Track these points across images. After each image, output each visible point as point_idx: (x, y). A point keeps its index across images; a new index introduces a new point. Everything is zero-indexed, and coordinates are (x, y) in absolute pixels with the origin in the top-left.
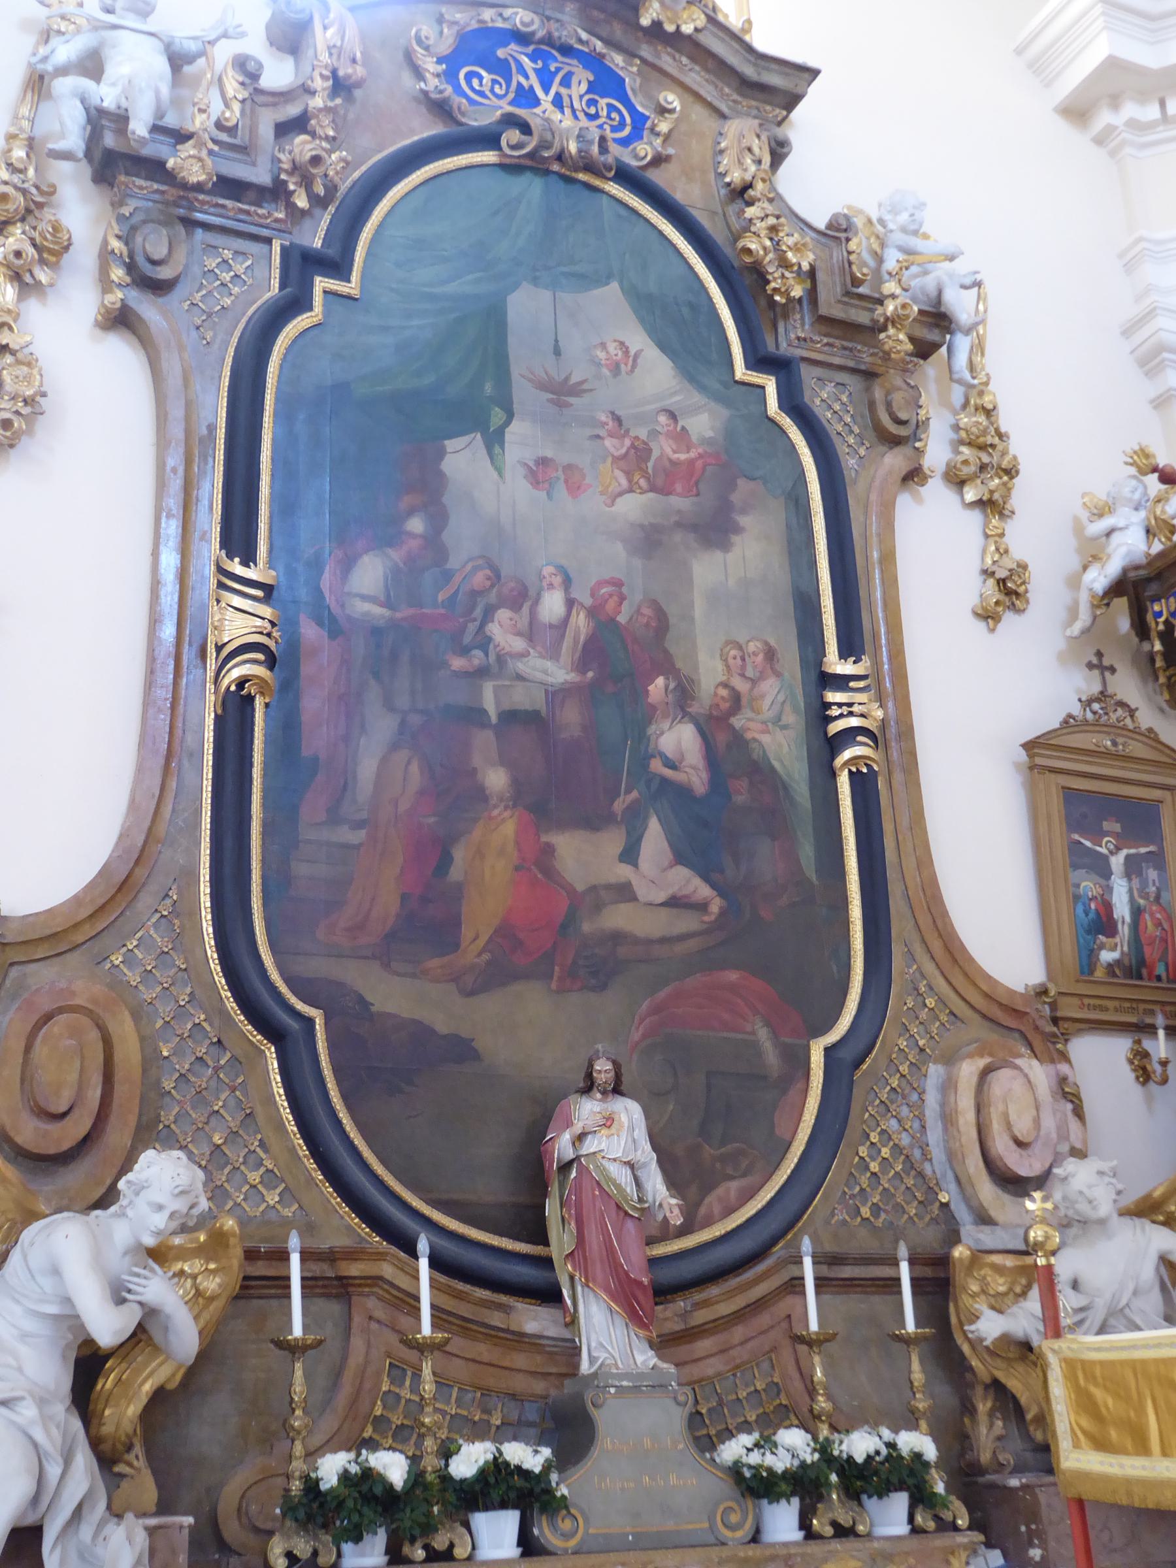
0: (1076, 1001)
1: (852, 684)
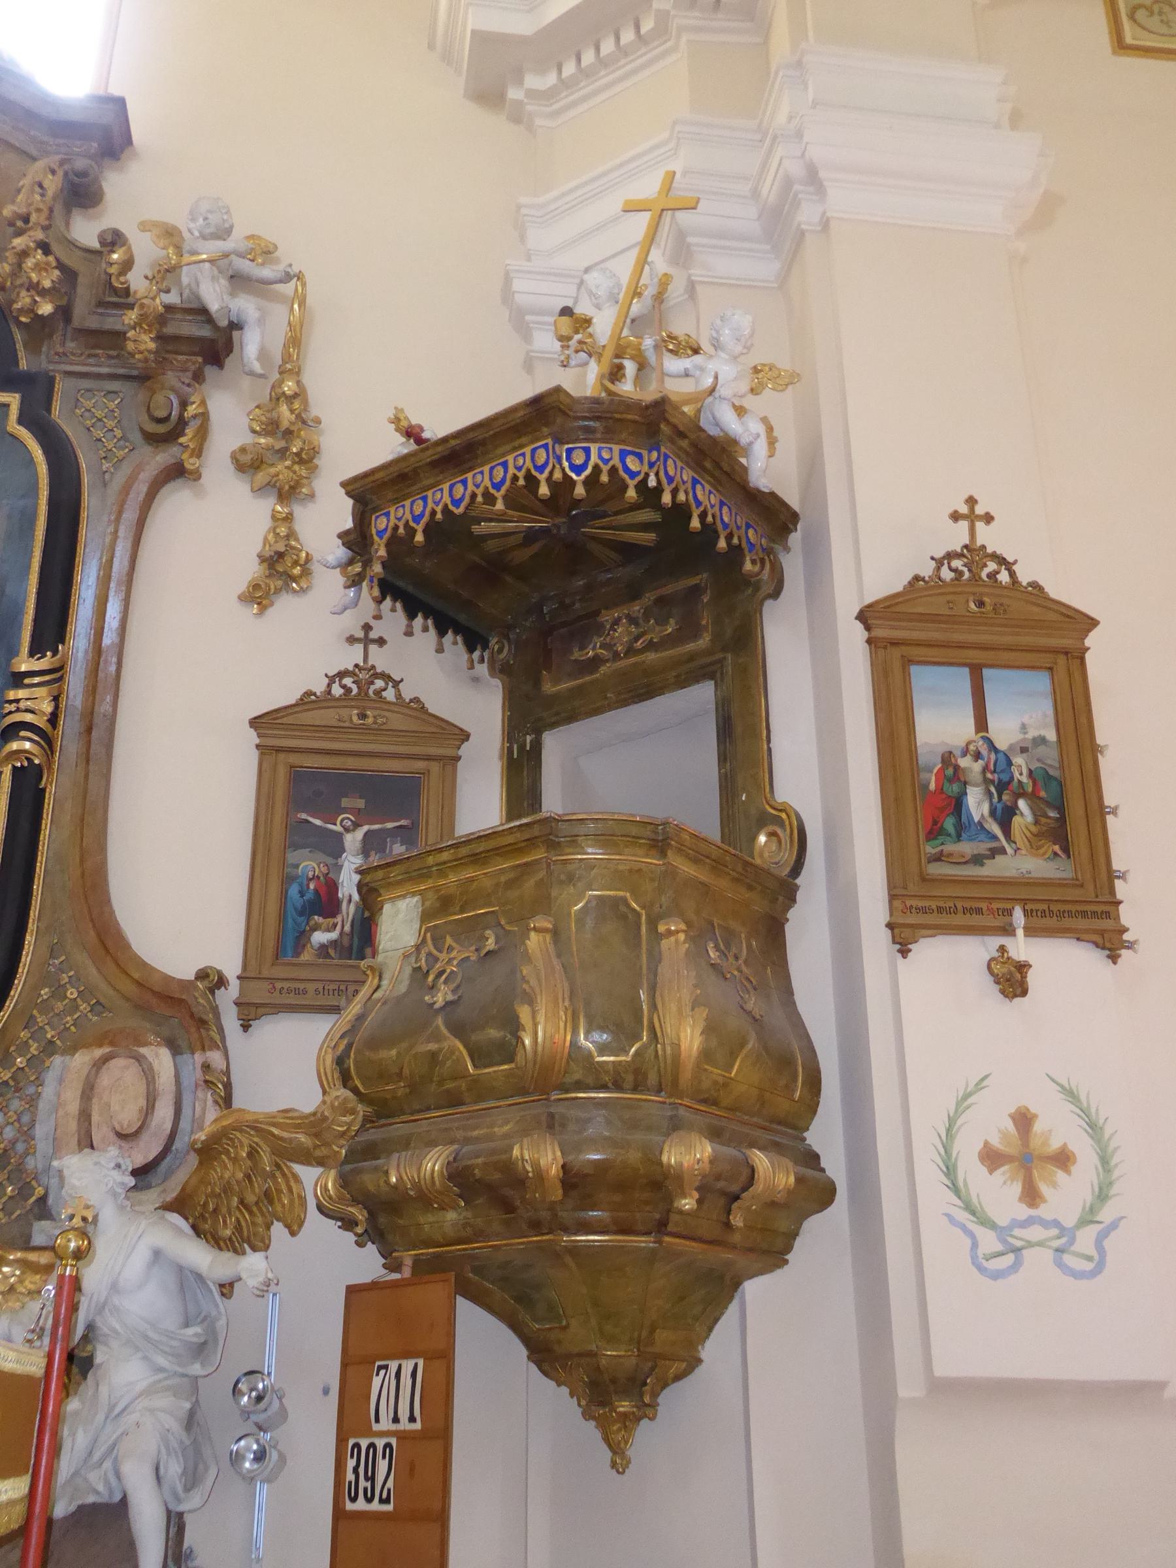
0: (266, 985)
1: (27, 681)
